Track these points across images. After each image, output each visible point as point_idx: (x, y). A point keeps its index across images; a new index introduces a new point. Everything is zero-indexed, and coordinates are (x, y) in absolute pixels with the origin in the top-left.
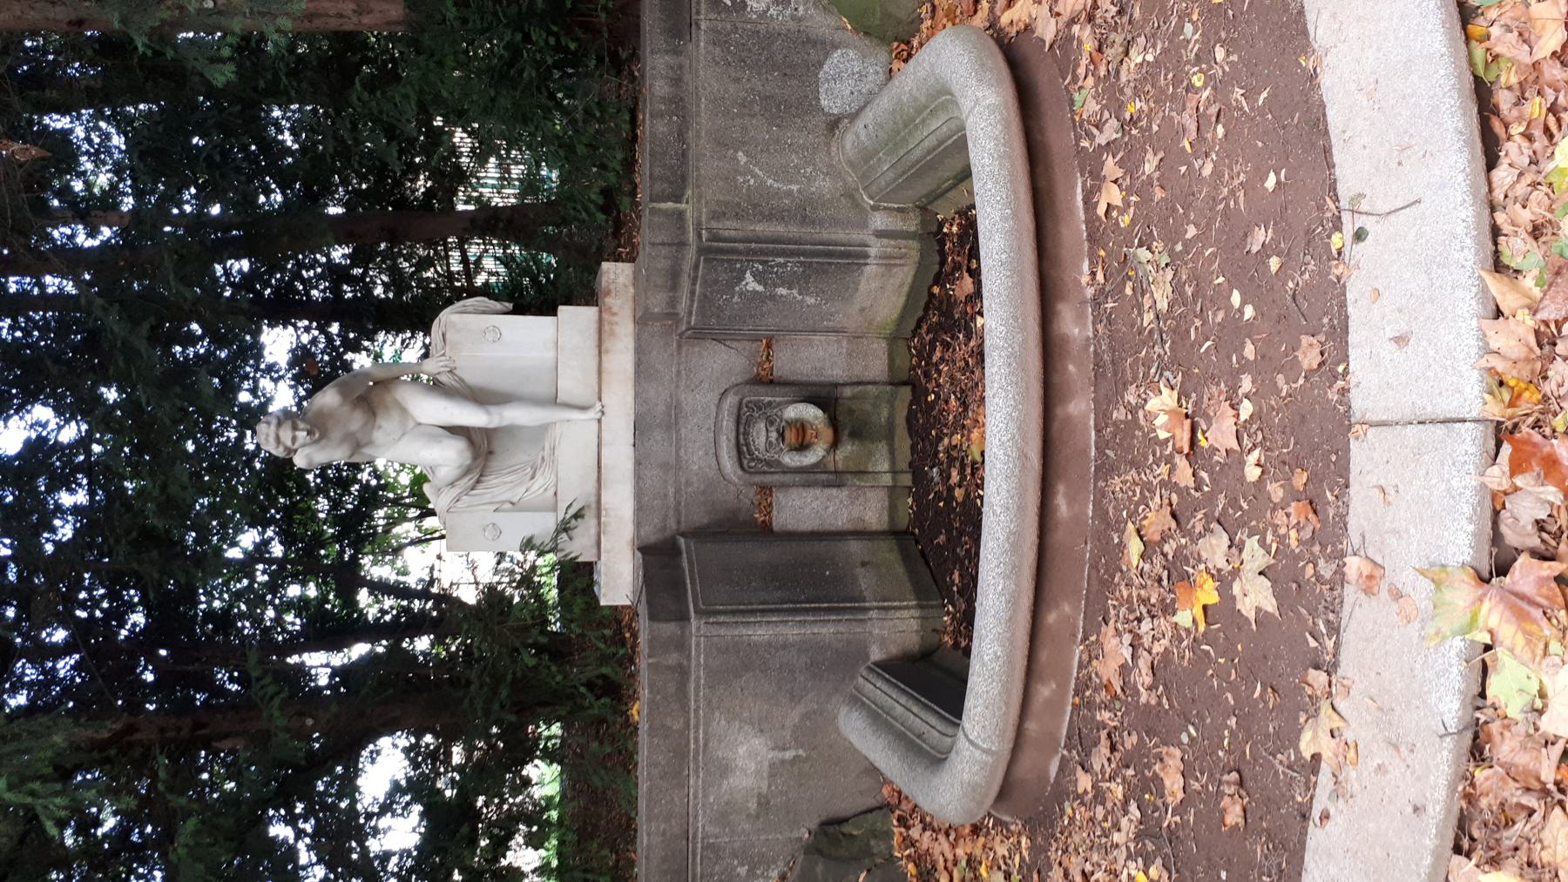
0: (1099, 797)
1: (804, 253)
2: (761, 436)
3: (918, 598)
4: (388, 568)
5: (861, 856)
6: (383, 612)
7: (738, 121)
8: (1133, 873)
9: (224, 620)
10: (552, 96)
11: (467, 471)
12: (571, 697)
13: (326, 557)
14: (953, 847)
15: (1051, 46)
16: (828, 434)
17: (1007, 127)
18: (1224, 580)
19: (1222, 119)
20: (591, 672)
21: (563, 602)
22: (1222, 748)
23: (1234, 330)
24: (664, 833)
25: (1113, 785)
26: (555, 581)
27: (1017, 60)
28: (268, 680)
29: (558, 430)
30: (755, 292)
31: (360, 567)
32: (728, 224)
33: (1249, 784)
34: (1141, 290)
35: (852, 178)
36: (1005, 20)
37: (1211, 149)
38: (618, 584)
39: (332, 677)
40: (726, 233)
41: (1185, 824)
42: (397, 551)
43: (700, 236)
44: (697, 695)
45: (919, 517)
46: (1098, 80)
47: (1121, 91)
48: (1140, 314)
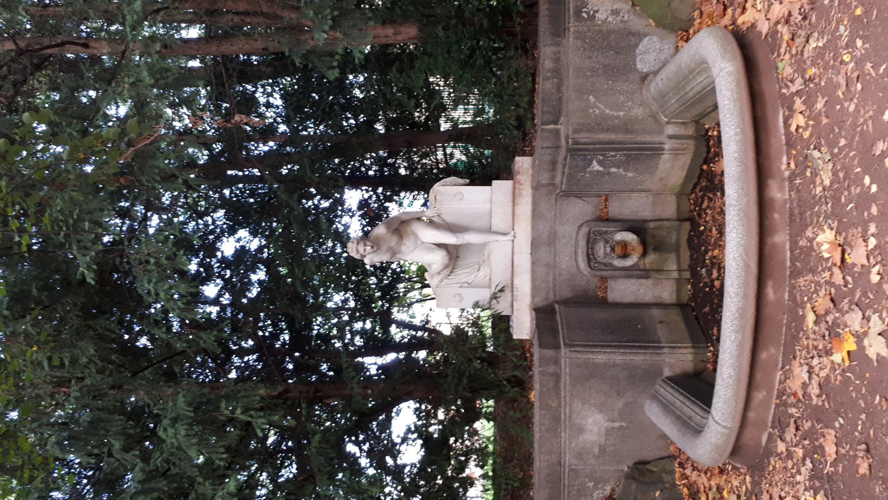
0: (790, 455)
1: (626, 149)
2: (601, 250)
3: (693, 342)
4: (405, 314)
5: (657, 482)
6: (403, 337)
7: (591, 80)
8: (808, 498)
9: (326, 338)
10: (491, 71)
11: (446, 267)
12: (499, 386)
13: (375, 308)
14: (709, 480)
15: (766, 36)
16: (639, 249)
17: (738, 84)
18: (859, 338)
19: (860, 80)
20: (509, 374)
21: (495, 336)
22: (858, 431)
23: (865, 199)
24: (548, 461)
25: (797, 449)
26: (490, 324)
27: (747, 48)
28: (350, 369)
29: (491, 246)
30: (598, 171)
31: (391, 313)
32: (584, 135)
33: (873, 452)
34: (815, 174)
35: (655, 107)
36: (740, 21)
37: (854, 96)
38: (523, 327)
39: (378, 370)
40: (583, 140)
41: (836, 472)
42: (410, 305)
43: (568, 142)
44: (565, 388)
45: (694, 297)
46: (792, 56)
47: (804, 62)
48: (815, 187)
